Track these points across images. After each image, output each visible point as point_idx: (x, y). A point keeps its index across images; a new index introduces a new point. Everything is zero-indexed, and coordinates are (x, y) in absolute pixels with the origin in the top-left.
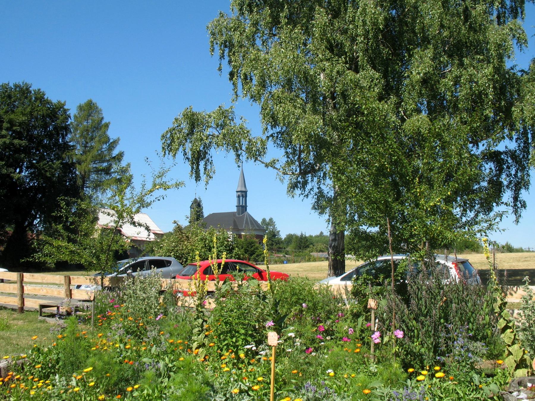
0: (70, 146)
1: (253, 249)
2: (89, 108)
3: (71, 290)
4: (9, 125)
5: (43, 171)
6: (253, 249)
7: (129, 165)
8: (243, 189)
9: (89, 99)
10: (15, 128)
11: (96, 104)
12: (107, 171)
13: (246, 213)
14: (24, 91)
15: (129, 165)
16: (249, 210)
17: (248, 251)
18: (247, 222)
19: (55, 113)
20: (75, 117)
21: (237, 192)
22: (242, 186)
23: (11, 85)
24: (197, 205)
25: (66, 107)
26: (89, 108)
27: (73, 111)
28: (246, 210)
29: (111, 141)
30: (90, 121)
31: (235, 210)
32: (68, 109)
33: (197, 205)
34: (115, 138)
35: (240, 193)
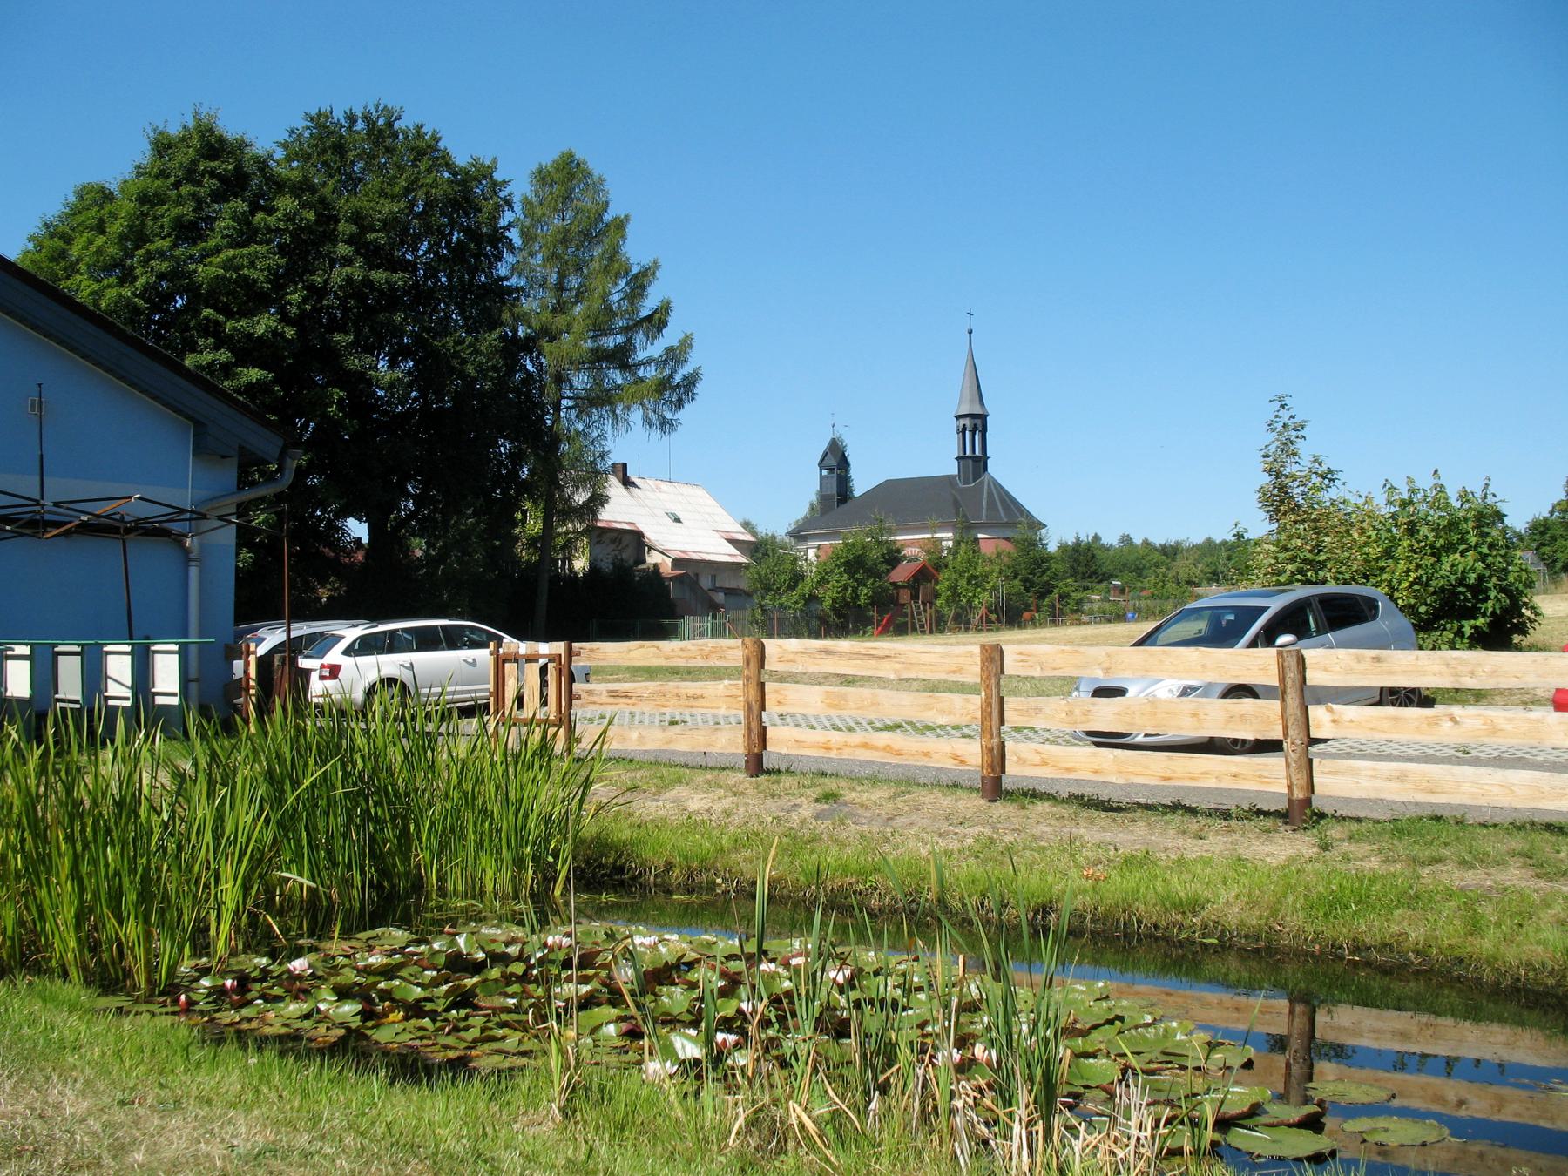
0: (510, 290)
1: (1045, 578)
2: (566, 177)
3: (763, 684)
4: (354, 228)
5: (454, 362)
6: (1045, 578)
7: (686, 343)
8: (977, 410)
9: (565, 150)
10: (370, 236)
11: (585, 163)
12: (621, 358)
13: (985, 477)
14: (381, 132)
15: (686, 343)
16: (995, 469)
17: (1032, 584)
18: (992, 504)
19: (467, 196)
20: (526, 202)
21: (958, 417)
23: (339, 115)
24: (836, 461)
25: (40, 232)
26: (566, 177)
27: (519, 184)
28: (986, 469)
29: (635, 270)
30: (569, 214)
32: (504, 182)
33: (836, 461)
34: (646, 261)
35: (967, 421)
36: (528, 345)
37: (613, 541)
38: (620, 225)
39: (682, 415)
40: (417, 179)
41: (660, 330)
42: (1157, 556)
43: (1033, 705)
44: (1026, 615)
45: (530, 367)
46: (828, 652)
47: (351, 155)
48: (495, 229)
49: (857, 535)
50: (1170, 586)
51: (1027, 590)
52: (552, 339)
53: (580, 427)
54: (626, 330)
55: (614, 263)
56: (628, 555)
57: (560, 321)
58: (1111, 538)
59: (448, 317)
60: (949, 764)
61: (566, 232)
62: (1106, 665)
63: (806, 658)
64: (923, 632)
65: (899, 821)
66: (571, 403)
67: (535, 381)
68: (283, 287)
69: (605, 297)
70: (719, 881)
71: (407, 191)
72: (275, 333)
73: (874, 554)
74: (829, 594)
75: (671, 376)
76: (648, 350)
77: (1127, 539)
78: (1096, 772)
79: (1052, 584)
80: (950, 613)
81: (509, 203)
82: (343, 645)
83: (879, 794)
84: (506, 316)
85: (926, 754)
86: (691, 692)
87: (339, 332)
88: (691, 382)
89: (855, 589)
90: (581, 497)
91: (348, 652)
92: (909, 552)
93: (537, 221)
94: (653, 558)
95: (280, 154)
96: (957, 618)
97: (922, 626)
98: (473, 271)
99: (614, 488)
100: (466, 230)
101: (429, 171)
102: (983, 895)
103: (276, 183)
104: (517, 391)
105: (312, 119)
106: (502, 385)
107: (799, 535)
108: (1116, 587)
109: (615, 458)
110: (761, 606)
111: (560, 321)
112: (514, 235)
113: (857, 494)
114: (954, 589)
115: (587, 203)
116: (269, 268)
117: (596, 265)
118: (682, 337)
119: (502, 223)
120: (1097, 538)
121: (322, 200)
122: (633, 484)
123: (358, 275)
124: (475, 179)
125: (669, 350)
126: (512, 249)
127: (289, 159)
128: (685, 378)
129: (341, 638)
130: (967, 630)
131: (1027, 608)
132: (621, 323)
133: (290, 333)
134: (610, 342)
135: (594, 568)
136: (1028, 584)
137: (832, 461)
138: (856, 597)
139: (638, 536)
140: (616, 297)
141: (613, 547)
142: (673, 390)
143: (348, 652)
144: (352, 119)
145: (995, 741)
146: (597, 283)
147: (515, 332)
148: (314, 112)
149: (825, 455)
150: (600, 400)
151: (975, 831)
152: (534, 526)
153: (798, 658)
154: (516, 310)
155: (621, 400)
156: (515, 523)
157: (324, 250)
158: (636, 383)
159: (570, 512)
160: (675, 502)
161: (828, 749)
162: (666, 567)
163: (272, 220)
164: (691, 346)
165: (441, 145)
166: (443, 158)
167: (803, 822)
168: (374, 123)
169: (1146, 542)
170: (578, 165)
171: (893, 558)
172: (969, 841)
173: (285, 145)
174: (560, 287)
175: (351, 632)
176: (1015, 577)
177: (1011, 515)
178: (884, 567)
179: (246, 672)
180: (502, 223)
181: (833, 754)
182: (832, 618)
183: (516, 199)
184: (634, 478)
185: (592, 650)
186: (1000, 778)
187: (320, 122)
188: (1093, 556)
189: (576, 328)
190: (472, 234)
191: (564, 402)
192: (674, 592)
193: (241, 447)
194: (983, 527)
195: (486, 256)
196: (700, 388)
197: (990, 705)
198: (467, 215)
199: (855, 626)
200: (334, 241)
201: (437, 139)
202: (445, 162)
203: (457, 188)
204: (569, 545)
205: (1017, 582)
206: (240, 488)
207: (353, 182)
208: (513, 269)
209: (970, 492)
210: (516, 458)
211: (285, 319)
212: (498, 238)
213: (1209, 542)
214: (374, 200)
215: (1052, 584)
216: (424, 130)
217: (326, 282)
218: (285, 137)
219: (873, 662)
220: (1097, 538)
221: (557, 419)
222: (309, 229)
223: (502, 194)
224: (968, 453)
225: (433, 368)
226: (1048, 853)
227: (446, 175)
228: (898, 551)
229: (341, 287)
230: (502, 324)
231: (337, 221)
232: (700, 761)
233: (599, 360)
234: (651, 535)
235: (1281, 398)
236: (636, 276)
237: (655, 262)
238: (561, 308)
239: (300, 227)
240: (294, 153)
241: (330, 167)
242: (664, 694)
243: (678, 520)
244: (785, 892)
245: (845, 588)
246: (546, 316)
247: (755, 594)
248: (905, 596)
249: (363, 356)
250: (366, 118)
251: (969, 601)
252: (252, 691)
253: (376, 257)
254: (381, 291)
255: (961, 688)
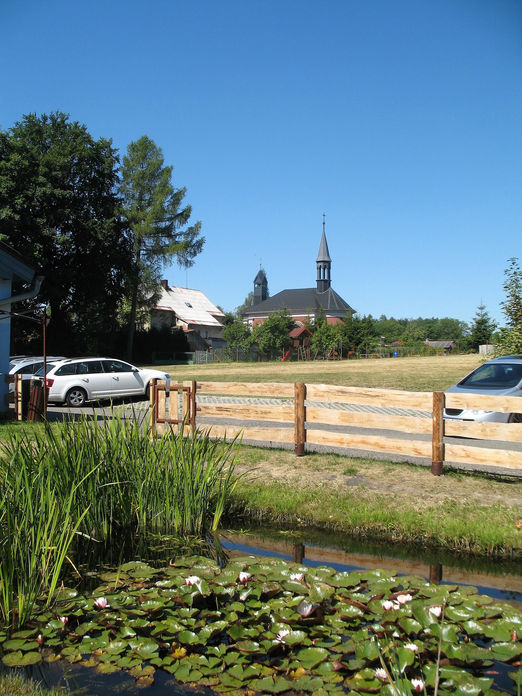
0: (118, 200)
1: (359, 336)
2: (144, 148)
4: (47, 169)
5: (92, 233)
7: (198, 226)
10: (54, 173)
11: (153, 142)
12: (168, 232)
13: (329, 289)
14: (59, 126)
15: (198, 226)
17: (353, 339)
19: (98, 157)
20: (125, 159)
21: (318, 262)
22: (324, 255)
23: (39, 117)
24: (261, 281)
25: (113, 147)
26: (144, 148)
27: (122, 151)
28: (330, 286)
29: (175, 191)
31: (315, 285)
32: (116, 150)
33: (261, 281)
34: (180, 188)
35: (321, 264)
36: (126, 225)
37: (161, 316)
38: (169, 171)
39: (195, 259)
40: (76, 147)
41: (186, 220)
42: (399, 326)
43: (462, 426)
44: (350, 353)
45: (125, 236)
46: (343, 392)
47: (45, 136)
48: (111, 171)
49: (276, 314)
50: (410, 341)
51: (350, 341)
52: (137, 223)
53: (149, 263)
54: (170, 219)
55: (165, 189)
56: (168, 322)
57: (141, 214)
58: (376, 317)
59: (88, 211)
60: (413, 454)
61: (144, 173)
62: (506, 406)
63: (330, 395)
64: (305, 360)
65: (396, 488)
66: (145, 252)
67: (128, 242)
68: (14, 196)
69: (162, 204)
70: (299, 520)
71: (71, 153)
72: (10, 217)
73: (282, 324)
74: (262, 343)
75: (191, 241)
76: (181, 228)
77: (384, 318)
78: (498, 462)
79: (359, 338)
80: (316, 351)
81: (117, 159)
82: (54, 370)
83: (376, 470)
84: (116, 212)
85: (399, 448)
86: (263, 410)
87: (40, 217)
88: (200, 244)
89: (274, 340)
90: (149, 296)
91: (57, 373)
92: (298, 323)
93: (130, 169)
94: (179, 324)
95: (11, 134)
96: (320, 354)
97: (304, 357)
98: (101, 190)
99: (164, 293)
100: (97, 172)
101: (81, 143)
102: (461, 537)
103: (10, 147)
104: (120, 246)
105: (27, 118)
106: (114, 243)
107: (244, 313)
108: (382, 339)
109: (164, 278)
110: (231, 347)
111: (141, 214)
112: (120, 174)
113: (271, 295)
114: (320, 341)
115: (154, 160)
116: (7, 187)
117: (157, 189)
118: (196, 223)
119: (114, 169)
120: (370, 316)
121: (32, 156)
122: (170, 290)
123: (49, 191)
124: (102, 148)
125: (190, 229)
126: (118, 181)
127: (16, 136)
128: (197, 242)
129: (54, 366)
130: (325, 359)
131: (350, 349)
132: (168, 216)
133: (17, 217)
134: (163, 225)
135: (153, 329)
136: (351, 338)
137: (260, 281)
138: (275, 343)
139: (173, 313)
140: (166, 204)
141: (161, 318)
142: (192, 247)
143: (57, 373)
144: (45, 118)
145: (441, 443)
146: (159, 199)
147: (119, 219)
148: (27, 115)
149: (257, 278)
150: (159, 251)
151: (442, 495)
152: (127, 308)
153: (325, 394)
154: (121, 209)
155: (168, 251)
156: (117, 307)
157: (33, 179)
158: (175, 244)
159: (144, 302)
160: (191, 299)
161: (342, 443)
162: (186, 328)
163: (8, 164)
164: (200, 227)
165: (87, 132)
166: (88, 138)
167: (340, 487)
168: (56, 121)
169: (392, 319)
170: (150, 143)
171: (291, 326)
172: (441, 503)
173: (14, 130)
174: (141, 199)
175: (59, 363)
176: (345, 335)
177: (342, 308)
178: (287, 330)
179: (16, 389)
180: (114, 169)
181: (345, 446)
182: (262, 353)
183: (121, 158)
184: (171, 287)
185: (208, 386)
186: (442, 463)
187: (30, 119)
188: (371, 325)
189: (148, 218)
190: (101, 174)
191: (142, 252)
192: (190, 339)
193: (14, 275)
194: (328, 312)
195: (106, 184)
196: (204, 247)
197: (438, 424)
198: (98, 164)
199: (274, 356)
200: (37, 175)
201: (85, 129)
202: (88, 139)
203: (94, 152)
204: (143, 317)
205: (346, 337)
206: (13, 295)
207: (45, 148)
208: (119, 190)
209: (323, 296)
210: (119, 277)
211: (15, 211)
212: (111, 176)
213: (420, 319)
214: (54, 156)
215: (359, 338)
216: (79, 125)
217: (34, 194)
218: (14, 126)
219: (369, 398)
220: (370, 316)
221: (138, 260)
222: (25, 169)
223: (114, 155)
224: (322, 278)
225: (82, 235)
226: (489, 511)
227: (89, 146)
228: (293, 323)
229: (40, 197)
230: (114, 216)
231: (38, 166)
232: (269, 445)
233: (158, 233)
234: (179, 312)
235: (512, 259)
236: (176, 194)
237: (185, 188)
238: (141, 208)
239: (21, 168)
240: (19, 133)
241: (35, 141)
242: (248, 410)
243: (190, 306)
244: (340, 528)
245: (270, 339)
246: (134, 213)
247: (225, 340)
248: (297, 343)
249: (51, 229)
250: (52, 118)
251: (327, 347)
252: (20, 399)
253: (56, 182)
254: (59, 199)
255: (422, 414)
